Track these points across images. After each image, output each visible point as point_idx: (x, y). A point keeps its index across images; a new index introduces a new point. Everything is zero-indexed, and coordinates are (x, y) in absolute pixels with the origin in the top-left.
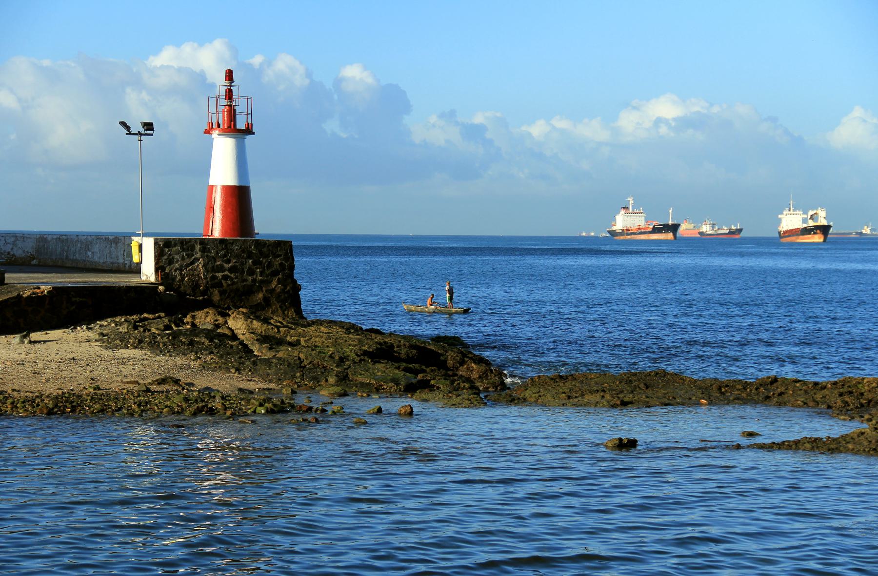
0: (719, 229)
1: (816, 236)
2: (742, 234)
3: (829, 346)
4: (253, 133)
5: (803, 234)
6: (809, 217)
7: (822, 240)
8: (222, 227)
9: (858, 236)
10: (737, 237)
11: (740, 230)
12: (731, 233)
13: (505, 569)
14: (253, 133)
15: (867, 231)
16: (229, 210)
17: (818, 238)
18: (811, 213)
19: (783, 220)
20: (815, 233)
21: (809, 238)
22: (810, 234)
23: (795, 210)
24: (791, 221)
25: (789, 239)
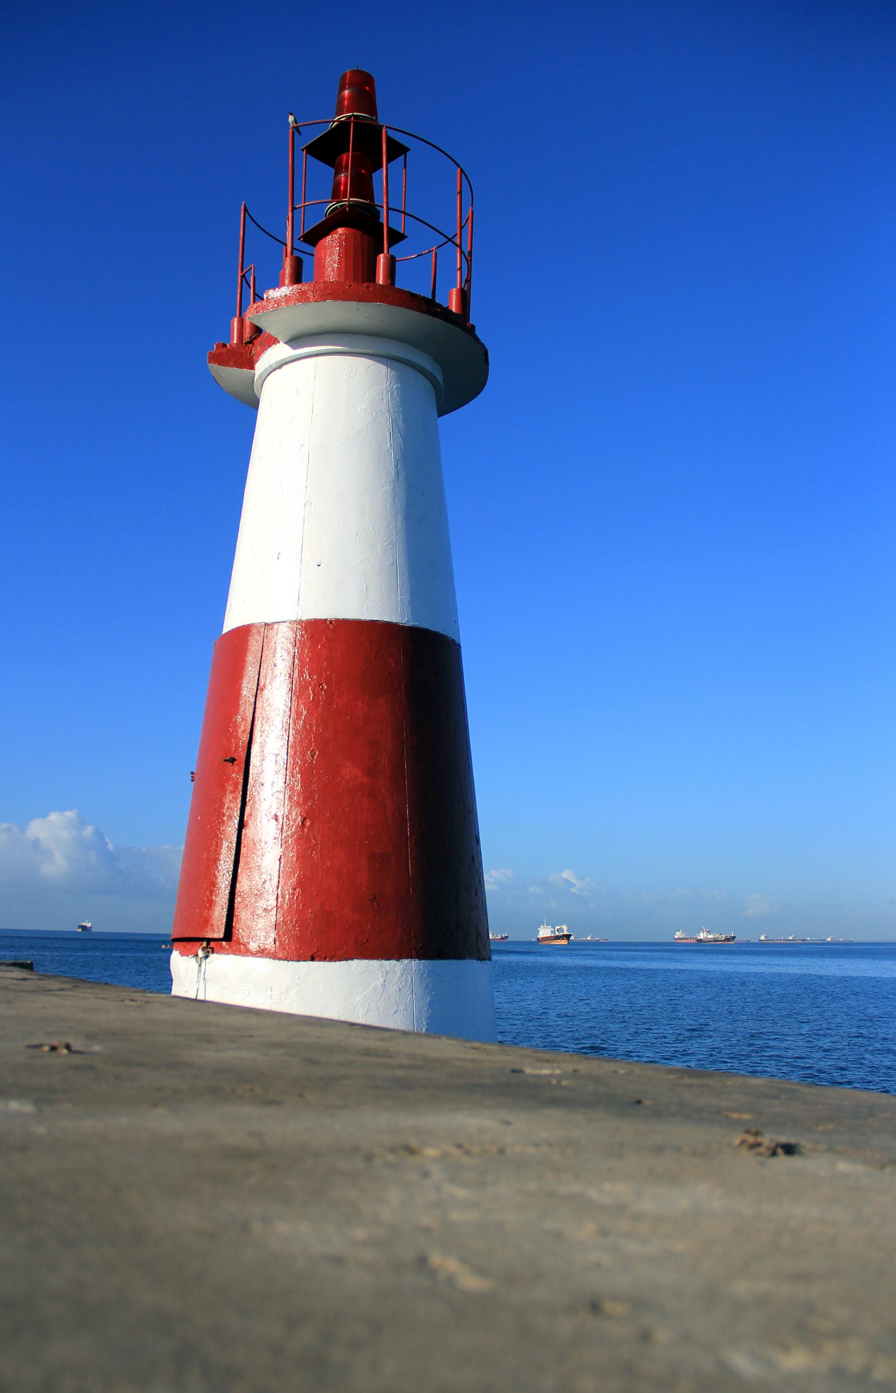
0: (496, 936)
1: (563, 941)
2: (509, 939)
3: (631, 1056)
4: (406, 237)
5: (555, 940)
6: (556, 930)
7: (567, 943)
8: (301, 883)
9: (80, 930)
10: (505, 941)
11: (734, 937)
12: (502, 938)
13: (344, 182)
14: (406, 237)
15: (762, 938)
16: (350, 772)
17: (564, 942)
18: (557, 927)
19: (540, 932)
20: (563, 939)
21: (559, 942)
22: (560, 939)
23: (547, 926)
24: (545, 932)
25: (545, 943)
